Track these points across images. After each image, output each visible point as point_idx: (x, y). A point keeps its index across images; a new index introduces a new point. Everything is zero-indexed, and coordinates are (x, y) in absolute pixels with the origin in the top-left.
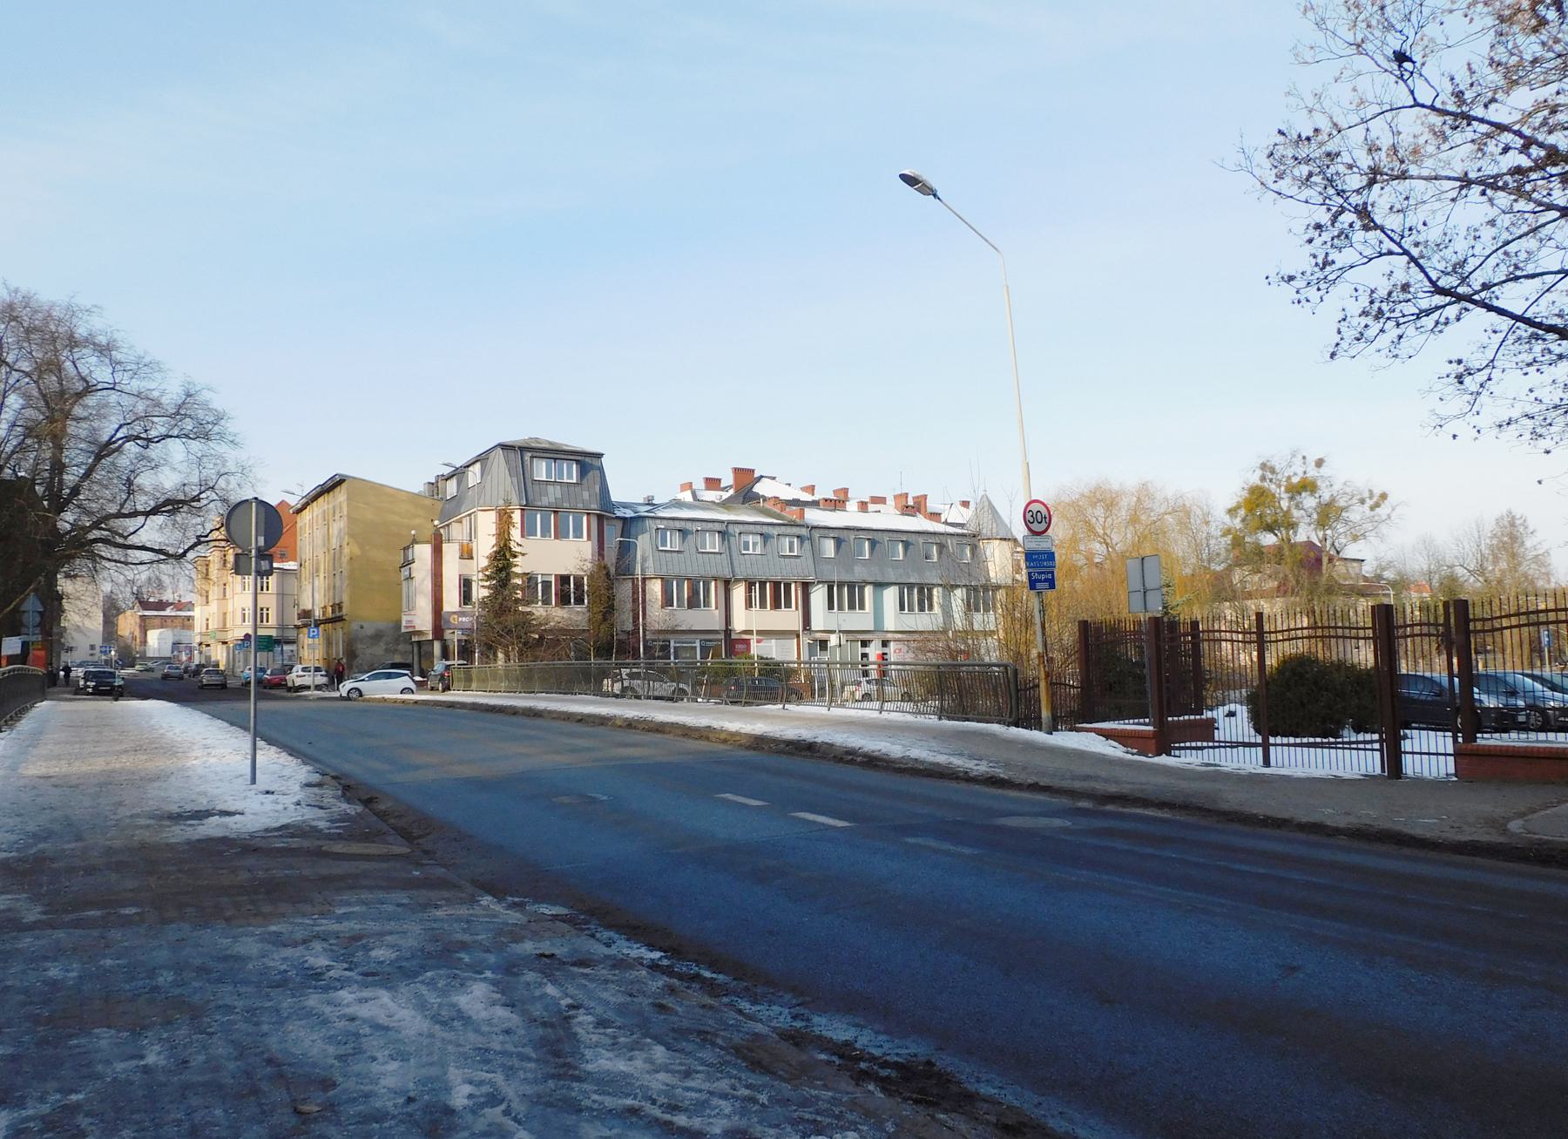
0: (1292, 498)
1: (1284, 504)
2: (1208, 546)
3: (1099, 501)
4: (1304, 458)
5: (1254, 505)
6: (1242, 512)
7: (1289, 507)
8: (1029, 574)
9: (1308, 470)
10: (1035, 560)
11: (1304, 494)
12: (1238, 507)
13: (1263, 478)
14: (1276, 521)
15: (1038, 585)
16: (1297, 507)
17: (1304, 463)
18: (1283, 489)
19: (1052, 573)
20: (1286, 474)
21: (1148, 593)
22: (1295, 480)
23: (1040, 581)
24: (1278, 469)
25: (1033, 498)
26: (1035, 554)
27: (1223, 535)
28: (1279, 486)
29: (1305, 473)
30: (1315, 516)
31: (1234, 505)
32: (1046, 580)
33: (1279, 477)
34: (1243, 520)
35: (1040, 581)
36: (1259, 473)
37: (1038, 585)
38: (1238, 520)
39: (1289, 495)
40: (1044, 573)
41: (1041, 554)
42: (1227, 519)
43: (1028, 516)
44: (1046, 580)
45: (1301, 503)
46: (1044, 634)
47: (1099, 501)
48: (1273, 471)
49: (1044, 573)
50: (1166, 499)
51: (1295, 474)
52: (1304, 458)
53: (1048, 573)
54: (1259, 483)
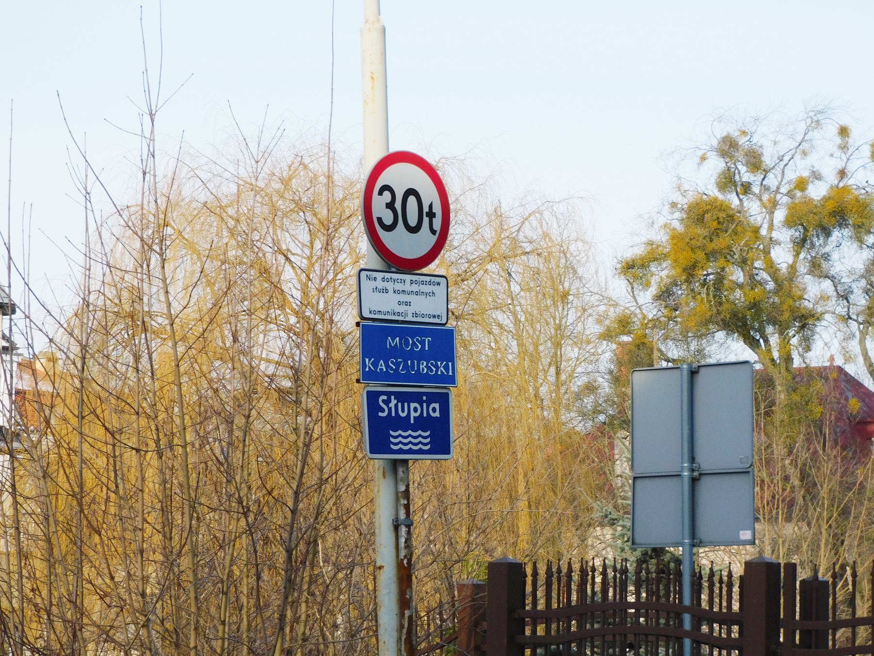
0: (801, 243)
1: (782, 256)
2: (556, 362)
3: (300, 207)
4: (844, 131)
5: (700, 255)
6: (662, 273)
7: (793, 268)
8: (372, 397)
9: (851, 168)
10: (394, 352)
11: (836, 234)
12: (653, 256)
13: (728, 181)
14: (755, 306)
15: (398, 438)
16: (817, 268)
17: (844, 148)
18: (780, 215)
19: (443, 400)
20: (791, 175)
21: (706, 485)
22: (817, 192)
23: (403, 424)
24: (768, 159)
25: (394, 148)
26: (394, 333)
27: (608, 336)
28: (774, 205)
29: (842, 174)
30: (860, 300)
31: (639, 251)
32: (422, 423)
33: (772, 181)
34: (664, 295)
35: (403, 424)
36: (716, 165)
37: (398, 438)
38: (646, 297)
39: (796, 233)
40: (416, 397)
41: (414, 333)
42: (619, 288)
43: (379, 203)
44: (422, 423)
45: (826, 257)
46: (404, 602)
47: (300, 207)
48: (755, 162)
49: (416, 397)
50: (498, 215)
51: (816, 176)
52: (844, 131)
53: (432, 398)
54: (714, 192)
